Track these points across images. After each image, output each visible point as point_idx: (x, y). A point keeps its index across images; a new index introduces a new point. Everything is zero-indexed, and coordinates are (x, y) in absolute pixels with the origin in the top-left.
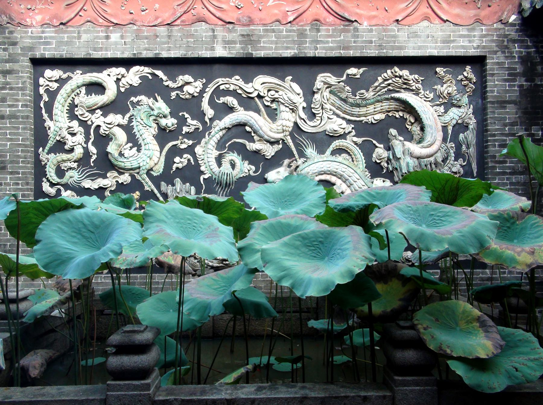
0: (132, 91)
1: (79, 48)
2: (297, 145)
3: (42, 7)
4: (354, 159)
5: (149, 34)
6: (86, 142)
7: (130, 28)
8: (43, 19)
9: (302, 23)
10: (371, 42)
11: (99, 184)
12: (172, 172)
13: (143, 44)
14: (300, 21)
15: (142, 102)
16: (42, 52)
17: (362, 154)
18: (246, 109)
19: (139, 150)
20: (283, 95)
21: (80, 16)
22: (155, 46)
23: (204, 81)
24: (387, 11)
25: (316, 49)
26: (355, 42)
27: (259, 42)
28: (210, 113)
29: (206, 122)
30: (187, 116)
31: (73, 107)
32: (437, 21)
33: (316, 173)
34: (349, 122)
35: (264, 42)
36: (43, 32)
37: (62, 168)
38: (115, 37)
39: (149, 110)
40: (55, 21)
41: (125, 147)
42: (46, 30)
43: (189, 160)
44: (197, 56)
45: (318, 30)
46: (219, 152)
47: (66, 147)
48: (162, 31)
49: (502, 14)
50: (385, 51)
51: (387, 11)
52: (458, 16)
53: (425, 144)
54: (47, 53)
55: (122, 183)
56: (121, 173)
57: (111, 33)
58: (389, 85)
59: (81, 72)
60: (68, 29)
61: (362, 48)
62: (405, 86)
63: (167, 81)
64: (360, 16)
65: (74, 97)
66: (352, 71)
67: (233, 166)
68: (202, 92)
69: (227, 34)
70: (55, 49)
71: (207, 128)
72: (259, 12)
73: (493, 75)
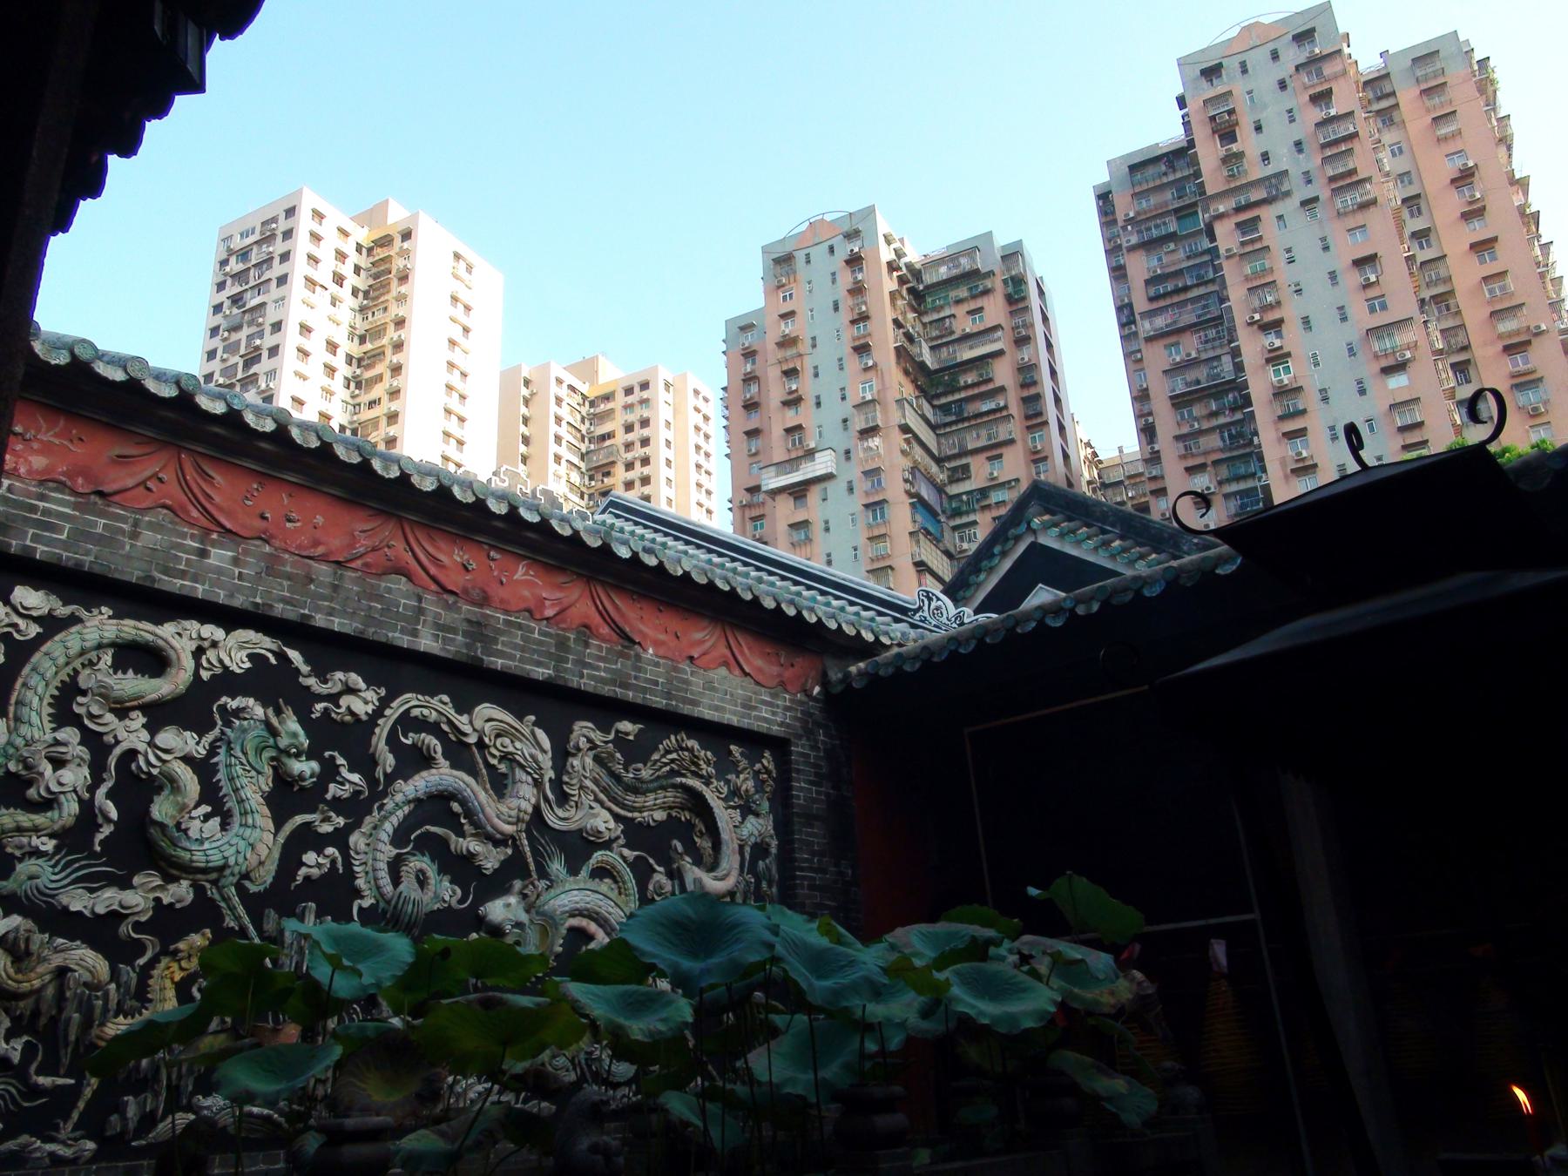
0: (228, 682)
1: (128, 557)
2: (536, 853)
3: (52, 439)
4: (622, 890)
5: (295, 571)
6: (92, 789)
7: (255, 546)
8: (47, 470)
9: (563, 626)
10: (656, 683)
11: (107, 903)
12: (293, 885)
13: (279, 588)
14: (564, 621)
15: (248, 713)
16: (28, 543)
17: (634, 881)
18: (454, 766)
19: (224, 826)
20: (522, 749)
21: (149, 489)
22: (304, 599)
23: (383, 692)
24: (678, 637)
25: (582, 676)
26: (636, 678)
27: (495, 641)
28: (388, 761)
29: (378, 781)
30: (341, 761)
31: (69, 691)
32: (737, 672)
33: (567, 912)
34: (617, 818)
35: (503, 644)
36: (42, 497)
37: (9, 850)
38: (220, 556)
39: (265, 734)
40: (80, 481)
41: (195, 813)
42: (53, 494)
43: (333, 862)
44: (384, 640)
45: (587, 645)
46: (396, 851)
47: (32, 793)
48: (323, 570)
49: (806, 681)
50: (674, 703)
51: (678, 637)
52: (760, 670)
53: (719, 873)
54: (41, 548)
55: (171, 905)
56: (169, 879)
57: (213, 547)
58: (673, 761)
59: (111, 613)
60: (111, 509)
61: (645, 690)
62: (693, 768)
63: (309, 676)
64: (644, 635)
65: (79, 667)
66: (626, 726)
67: (422, 881)
68: (378, 713)
69: (443, 613)
70: (65, 545)
71: (377, 792)
72: (499, 585)
73: (798, 771)
